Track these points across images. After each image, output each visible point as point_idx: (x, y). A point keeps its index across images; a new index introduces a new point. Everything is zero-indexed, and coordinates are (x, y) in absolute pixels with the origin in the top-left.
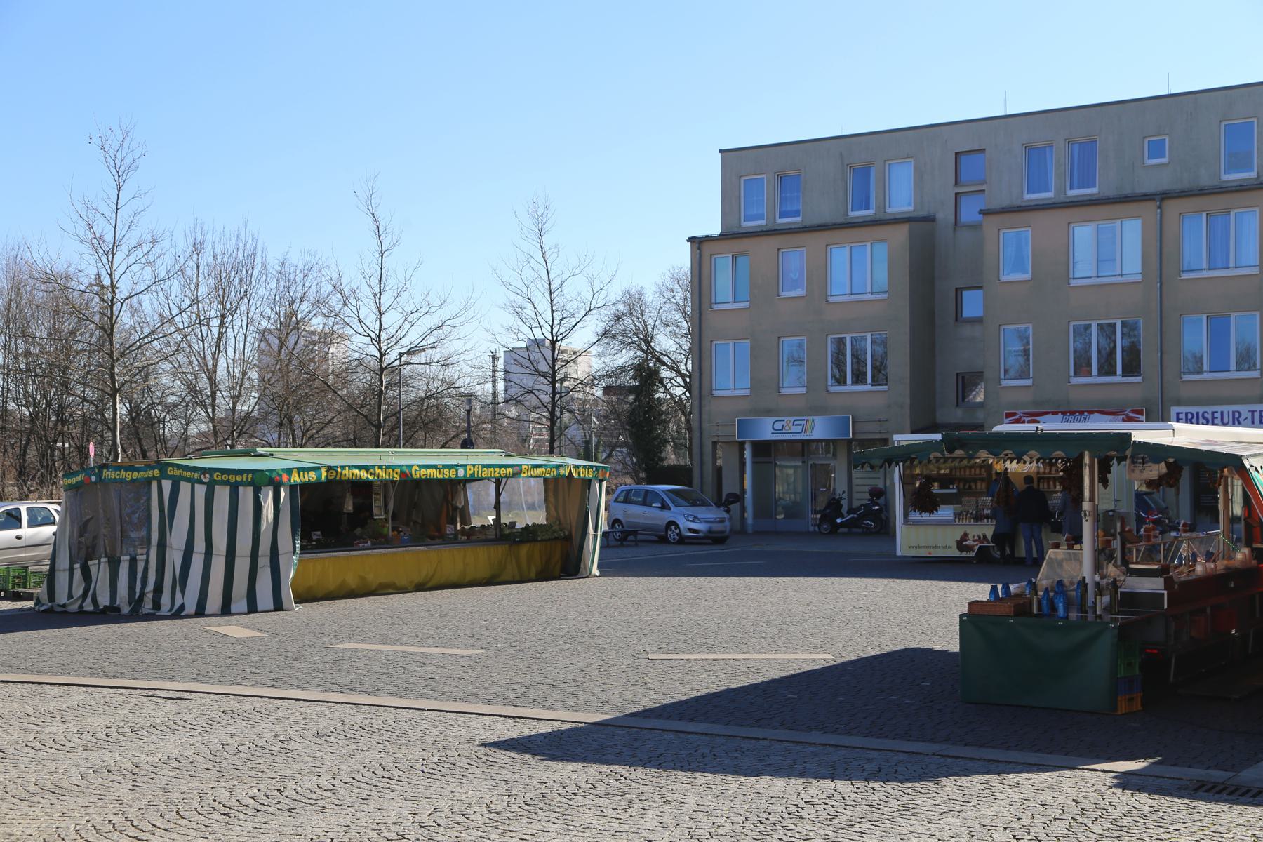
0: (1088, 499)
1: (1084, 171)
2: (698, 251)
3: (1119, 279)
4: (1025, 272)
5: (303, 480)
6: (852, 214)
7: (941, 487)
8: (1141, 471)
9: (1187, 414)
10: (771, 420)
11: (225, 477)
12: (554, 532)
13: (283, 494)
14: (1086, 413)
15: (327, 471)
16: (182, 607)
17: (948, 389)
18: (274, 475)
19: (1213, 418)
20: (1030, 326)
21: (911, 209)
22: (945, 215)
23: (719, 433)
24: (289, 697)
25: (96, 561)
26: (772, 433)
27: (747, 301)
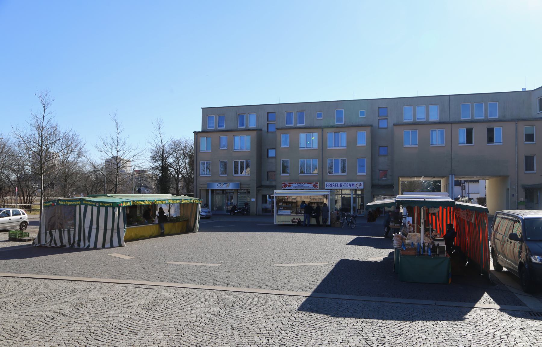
0: (423, 219)
1: (301, 121)
3: (312, 148)
4: (287, 145)
5: (126, 205)
6: (239, 127)
7: (286, 205)
8: (433, 210)
10: (217, 183)
11: (104, 204)
12: (184, 218)
13: (121, 209)
15: (133, 202)
16: (89, 246)
18: (119, 204)
19: (335, 185)
20: (289, 160)
21: (255, 127)
22: (265, 129)
23: (202, 187)
24: (190, 287)
25: (54, 230)
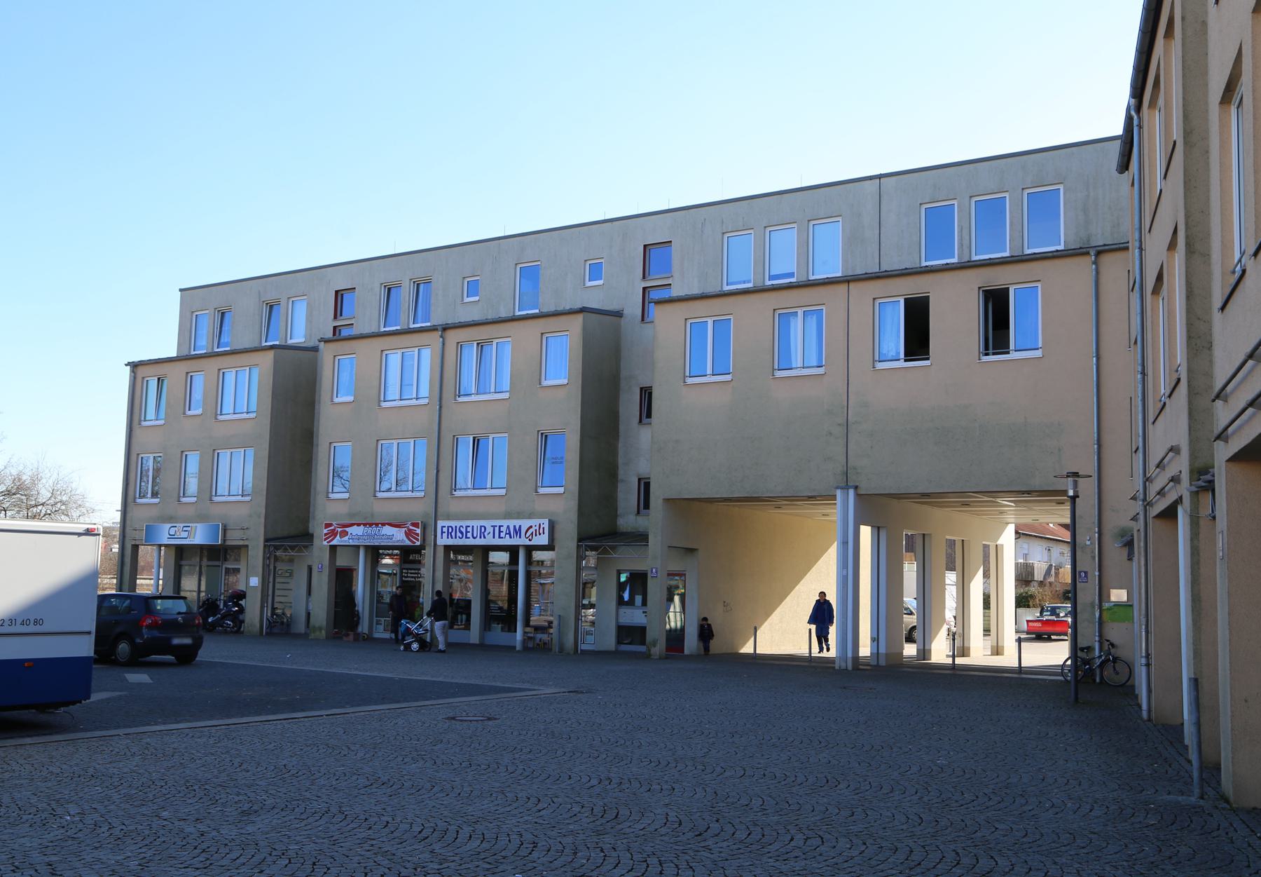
2: (441, 339)
9: (448, 527)
14: (380, 525)
17: (627, 497)
21: (303, 340)
26: (169, 538)
27: (507, 392)
